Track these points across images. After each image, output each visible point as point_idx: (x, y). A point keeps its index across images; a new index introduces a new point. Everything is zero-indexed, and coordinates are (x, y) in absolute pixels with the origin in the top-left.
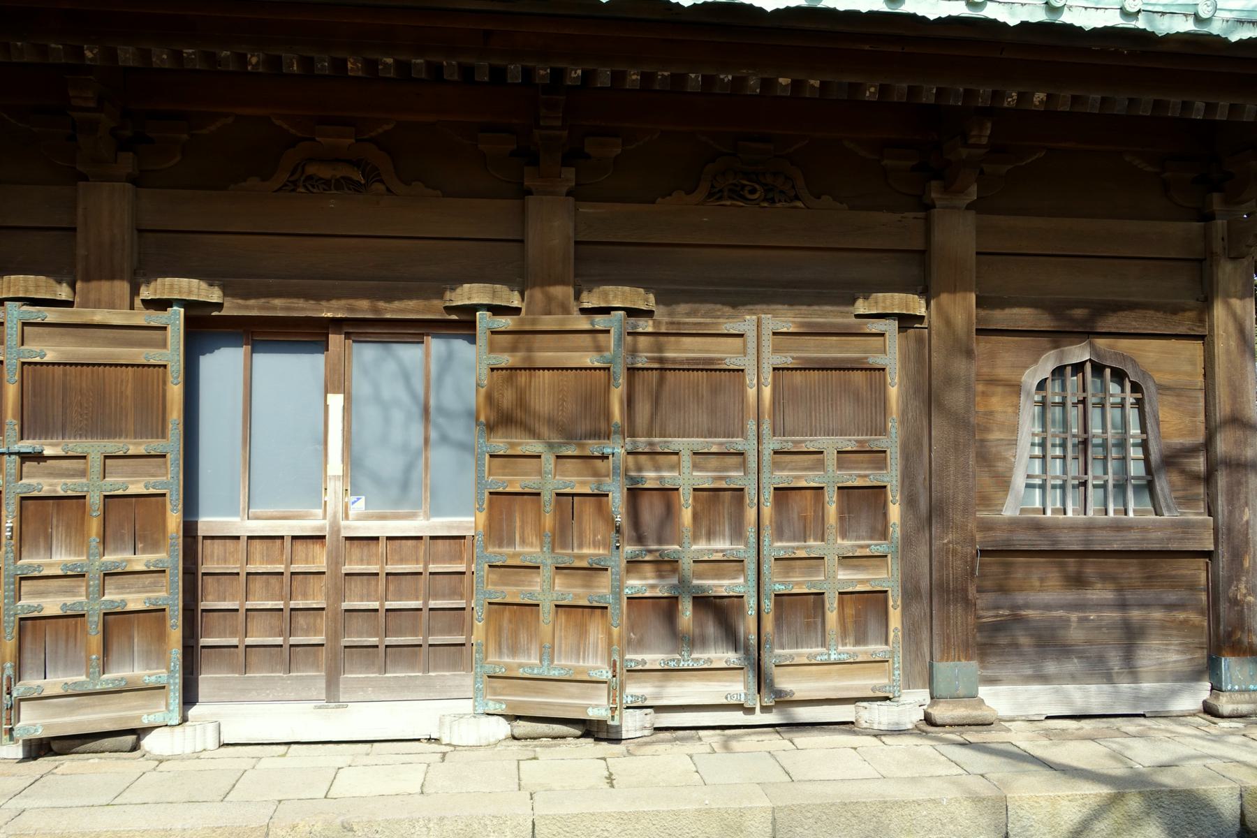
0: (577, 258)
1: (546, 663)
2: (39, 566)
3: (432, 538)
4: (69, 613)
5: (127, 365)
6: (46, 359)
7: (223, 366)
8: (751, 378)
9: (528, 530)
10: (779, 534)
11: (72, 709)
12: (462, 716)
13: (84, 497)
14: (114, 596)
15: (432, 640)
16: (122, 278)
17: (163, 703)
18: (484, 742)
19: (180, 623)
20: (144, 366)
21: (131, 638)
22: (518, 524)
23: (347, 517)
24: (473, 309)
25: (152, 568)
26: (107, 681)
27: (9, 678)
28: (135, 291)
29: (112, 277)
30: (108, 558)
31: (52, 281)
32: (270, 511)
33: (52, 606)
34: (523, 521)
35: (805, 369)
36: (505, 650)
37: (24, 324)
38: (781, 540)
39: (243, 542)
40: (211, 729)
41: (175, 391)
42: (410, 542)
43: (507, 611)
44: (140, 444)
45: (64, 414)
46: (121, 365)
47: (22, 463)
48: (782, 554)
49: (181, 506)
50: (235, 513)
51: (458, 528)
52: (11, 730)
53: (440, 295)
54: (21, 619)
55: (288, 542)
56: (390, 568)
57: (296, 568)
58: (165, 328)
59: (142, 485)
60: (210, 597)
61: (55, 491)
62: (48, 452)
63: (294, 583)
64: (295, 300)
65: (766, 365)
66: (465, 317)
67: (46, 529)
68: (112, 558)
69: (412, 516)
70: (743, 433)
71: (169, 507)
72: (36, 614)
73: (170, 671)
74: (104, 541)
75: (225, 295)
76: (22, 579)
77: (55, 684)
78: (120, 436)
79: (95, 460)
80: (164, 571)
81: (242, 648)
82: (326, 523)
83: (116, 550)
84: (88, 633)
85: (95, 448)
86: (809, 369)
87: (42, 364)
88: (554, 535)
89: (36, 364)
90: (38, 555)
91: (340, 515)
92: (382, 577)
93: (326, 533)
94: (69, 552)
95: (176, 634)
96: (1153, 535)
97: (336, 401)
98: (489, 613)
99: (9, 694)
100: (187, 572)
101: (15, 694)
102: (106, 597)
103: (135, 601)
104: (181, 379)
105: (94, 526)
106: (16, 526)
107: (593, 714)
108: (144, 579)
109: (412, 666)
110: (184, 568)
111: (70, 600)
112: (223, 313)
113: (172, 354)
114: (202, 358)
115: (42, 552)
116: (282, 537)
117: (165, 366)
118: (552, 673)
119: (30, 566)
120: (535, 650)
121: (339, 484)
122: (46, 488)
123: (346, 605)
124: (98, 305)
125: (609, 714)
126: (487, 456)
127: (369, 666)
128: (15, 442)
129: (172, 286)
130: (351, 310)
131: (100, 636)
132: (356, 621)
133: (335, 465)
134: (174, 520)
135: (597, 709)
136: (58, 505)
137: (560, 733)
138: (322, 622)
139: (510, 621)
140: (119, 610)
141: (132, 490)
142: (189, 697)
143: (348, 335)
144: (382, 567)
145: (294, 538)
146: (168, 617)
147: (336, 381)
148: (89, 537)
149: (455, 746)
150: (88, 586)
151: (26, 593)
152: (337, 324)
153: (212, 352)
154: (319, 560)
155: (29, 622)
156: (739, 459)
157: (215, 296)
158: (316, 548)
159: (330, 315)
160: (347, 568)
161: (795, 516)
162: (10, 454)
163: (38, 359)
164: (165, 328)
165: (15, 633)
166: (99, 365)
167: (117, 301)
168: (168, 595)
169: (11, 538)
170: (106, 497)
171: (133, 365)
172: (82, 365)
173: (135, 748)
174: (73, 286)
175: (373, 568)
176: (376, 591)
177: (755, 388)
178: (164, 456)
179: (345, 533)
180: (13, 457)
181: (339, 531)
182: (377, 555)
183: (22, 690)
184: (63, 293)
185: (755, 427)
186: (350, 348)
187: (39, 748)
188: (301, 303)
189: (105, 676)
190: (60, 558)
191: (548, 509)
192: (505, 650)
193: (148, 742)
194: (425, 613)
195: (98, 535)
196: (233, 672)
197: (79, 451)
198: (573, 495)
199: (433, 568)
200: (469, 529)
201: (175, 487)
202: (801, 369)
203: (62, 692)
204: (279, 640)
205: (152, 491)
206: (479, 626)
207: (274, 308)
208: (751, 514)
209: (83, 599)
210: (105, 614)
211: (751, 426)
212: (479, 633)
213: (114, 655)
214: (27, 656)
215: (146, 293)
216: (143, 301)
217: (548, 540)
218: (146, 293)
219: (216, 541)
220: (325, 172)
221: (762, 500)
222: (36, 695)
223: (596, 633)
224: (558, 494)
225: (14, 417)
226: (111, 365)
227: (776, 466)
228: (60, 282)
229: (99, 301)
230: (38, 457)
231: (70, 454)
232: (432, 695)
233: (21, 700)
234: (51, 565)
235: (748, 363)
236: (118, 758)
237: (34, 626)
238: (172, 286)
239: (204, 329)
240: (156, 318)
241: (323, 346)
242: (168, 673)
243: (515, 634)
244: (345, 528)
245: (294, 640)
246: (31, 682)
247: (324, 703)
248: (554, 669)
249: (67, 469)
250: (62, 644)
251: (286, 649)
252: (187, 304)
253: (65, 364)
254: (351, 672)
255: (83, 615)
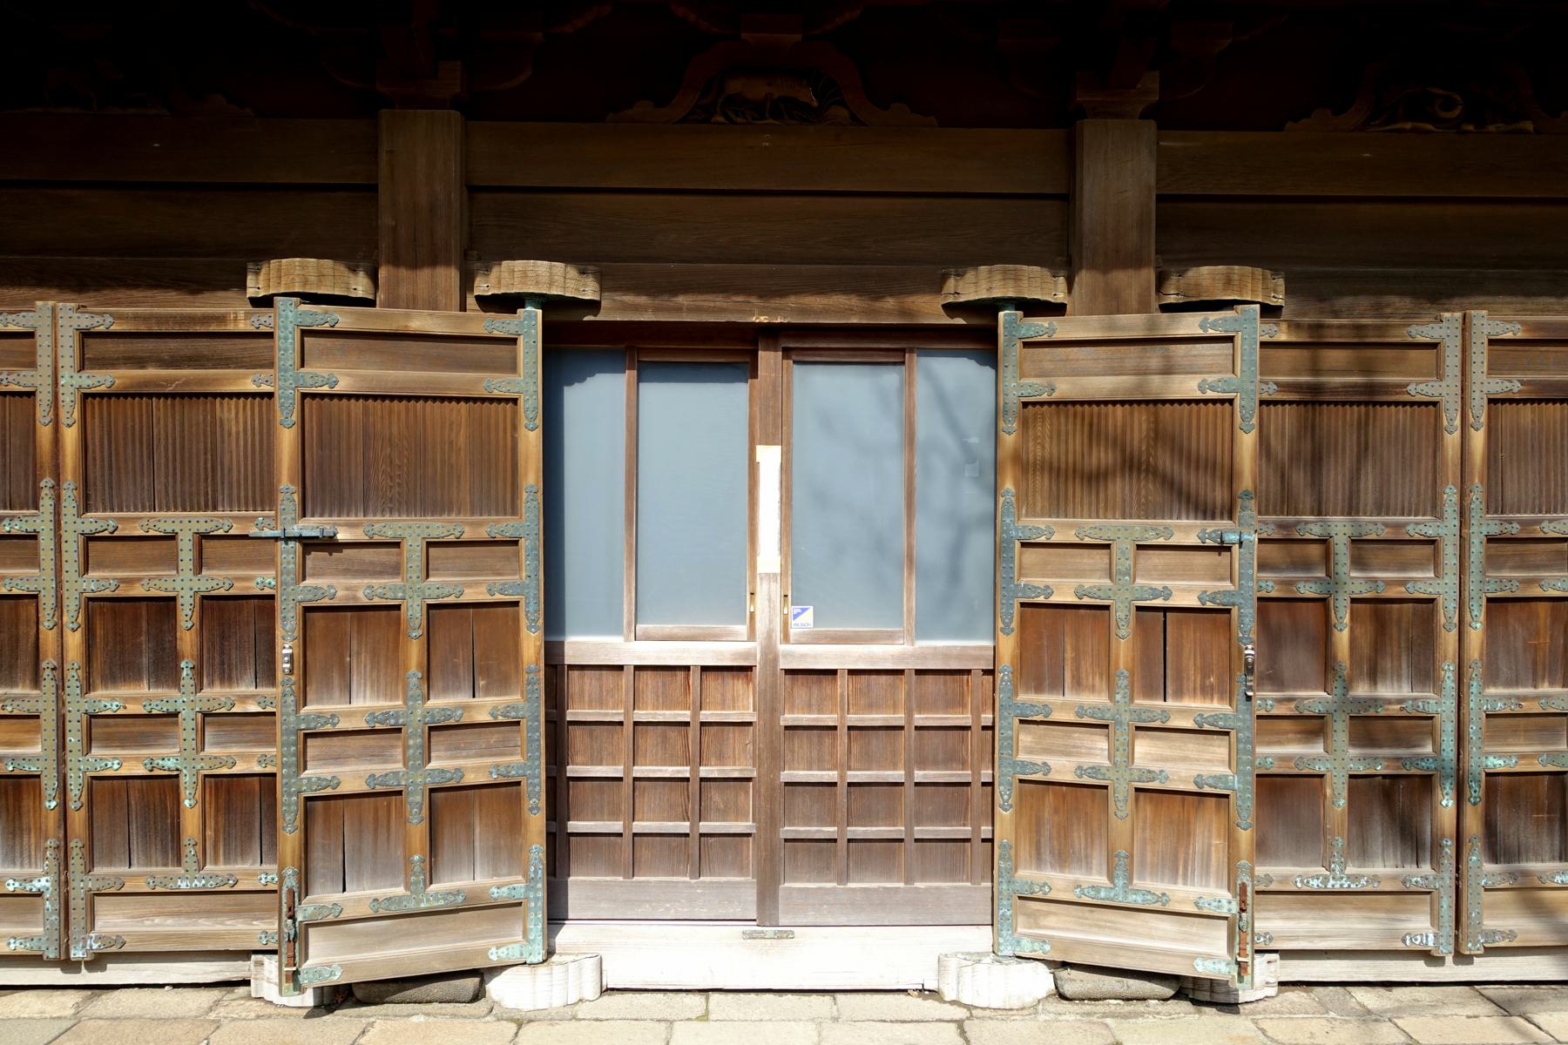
0: (1161, 226)
1: (1120, 882)
2: (333, 716)
3: (919, 672)
4: (379, 789)
5: (458, 400)
6: (338, 389)
7: (597, 400)
8: (1451, 418)
9: (1086, 665)
10: (1492, 677)
11: (384, 940)
12: (977, 958)
13: (398, 607)
14: (446, 763)
15: (921, 831)
16: (448, 263)
17: (519, 929)
18: (1016, 1004)
19: (543, 803)
20: (483, 400)
21: (470, 828)
22: (1069, 654)
23: (786, 638)
24: (990, 308)
25: (501, 719)
26: (436, 896)
27: (291, 892)
28: (466, 284)
29: (434, 262)
30: (436, 702)
31: (341, 268)
32: (668, 628)
33: (352, 776)
34: (1077, 650)
35: (1540, 401)
36: (1047, 857)
37: (305, 333)
38: (1495, 685)
39: (626, 678)
40: (590, 966)
41: (531, 440)
42: (883, 679)
43: (1050, 797)
44: (480, 524)
45: (366, 476)
46: (450, 399)
47: (305, 552)
48: (1500, 707)
49: (541, 621)
50: (617, 630)
51: (959, 657)
52: (296, 973)
53: (937, 286)
54: (307, 799)
55: (695, 677)
56: (855, 719)
57: (707, 715)
58: (513, 341)
59: (483, 589)
60: (579, 759)
61: (355, 598)
62: (342, 536)
63: (705, 739)
64: (710, 297)
65: (1477, 395)
66: (976, 321)
67: (342, 658)
68: (442, 703)
69: (889, 637)
70: (1435, 509)
71: (524, 622)
72: (329, 791)
73: (528, 880)
74: (428, 677)
75: (602, 290)
76: (307, 736)
77: (359, 900)
78: (450, 512)
79: (413, 551)
80: (518, 723)
81: (628, 838)
82: (755, 646)
83: (445, 691)
84: (406, 821)
85: (413, 530)
86: (1547, 401)
87: (332, 396)
88: (1132, 674)
89: (322, 396)
90: (330, 700)
91: (778, 635)
92: (842, 733)
93: (757, 662)
94: (377, 694)
95: (536, 822)
96: (1545, 640)
97: (769, 457)
98: (1021, 796)
99: (293, 917)
100: (550, 722)
101: (300, 918)
102: (433, 765)
103: (475, 767)
104: (539, 421)
105: (414, 652)
106: (298, 652)
107: (1203, 969)
108: (486, 731)
109: (887, 872)
110: (547, 714)
111: (378, 768)
112: (599, 318)
113: (524, 379)
114: (566, 389)
115: (337, 693)
116: (687, 668)
117: (515, 401)
118: (1131, 898)
119: (319, 715)
120: (1098, 858)
121: (776, 588)
122: (340, 593)
123: (787, 775)
124: (413, 303)
125: (1234, 970)
126: (1018, 544)
127: (821, 872)
128: (295, 521)
129: (525, 274)
130: (1111, 327)
131: (425, 825)
132: (802, 800)
133: (769, 557)
134: (531, 643)
135: (1207, 954)
136: (360, 620)
137: (1140, 994)
138: (749, 799)
139: (1056, 811)
140: (453, 783)
141: (469, 596)
142: (556, 916)
143: (787, 353)
144: (842, 717)
145: (705, 669)
146: (525, 796)
147: (771, 423)
148: (406, 669)
149: (968, 1007)
150: (406, 748)
151: (314, 759)
152: (772, 335)
153: (582, 380)
154: (742, 705)
155: (319, 804)
156: (1428, 549)
157: (588, 290)
158: (737, 685)
159: (763, 319)
160: (789, 718)
161: (1519, 644)
162: (287, 539)
163: (325, 389)
164: (513, 341)
165: (299, 822)
166: (417, 398)
167: (442, 300)
168: (523, 761)
169: (291, 672)
170: (430, 607)
171: (467, 400)
172: (392, 398)
173: (478, 996)
174: (374, 277)
175: (828, 719)
176: (833, 754)
177: (1457, 434)
178: (516, 543)
179: (785, 664)
180: (291, 544)
181: (775, 660)
182: (833, 698)
183: (310, 910)
184: (359, 286)
185: (1455, 498)
186: (790, 373)
187: (336, 998)
188: (718, 301)
189: (434, 887)
190: (363, 704)
191: (1123, 632)
192: (1047, 857)
193: (495, 987)
194: (693, 732)
195: (419, 666)
196: (614, 874)
197: (389, 535)
198: (1165, 610)
199: (921, 719)
200: (977, 659)
201: (533, 592)
202: (1532, 401)
203: (369, 913)
204: (684, 826)
205: (498, 597)
206: (1004, 815)
207: (679, 309)
208: (1449, 639)
209: (399, 766)
210: (432, 791)
211: (1450, 495)
212: (1006, 823)
213: (446, 854)
214: (317, 855)
215: (485, 286)
216: (479, 299)
217: (1123, 682)
218: (485, 286)
219: (587, 673)
220: (758, 90)
221: (1468, 618)
222: (331, 918)
223: (1207, 835)
224: (1139, 608)
225: (292, 481)
226: (434, 399)
227: (1492, 562)
228: (354, 270)
229: (414, 298)
230: (328, 544)
231: (377, 539)
232: (921, 919)
233: (308, 926)
234: (350, 714)
235: (1445, 390)
236: (454, 1016)
237: (326, 809)
238: (525, 274)
239: (574, 342)
240: (498, 324)
241: (749, 370)
242: (521, 882)
243: (1064, 833)
244: (786, 655)
245: (706, 826)
246: (324, 897)
247: (752, 927)
248: (1136, 892)
249: (372, 563)
250: (368, 837)
251: (694, 842)
252: (549, 303)
253: (366, 397)
254: (795, 880)
255: (400, 793)
